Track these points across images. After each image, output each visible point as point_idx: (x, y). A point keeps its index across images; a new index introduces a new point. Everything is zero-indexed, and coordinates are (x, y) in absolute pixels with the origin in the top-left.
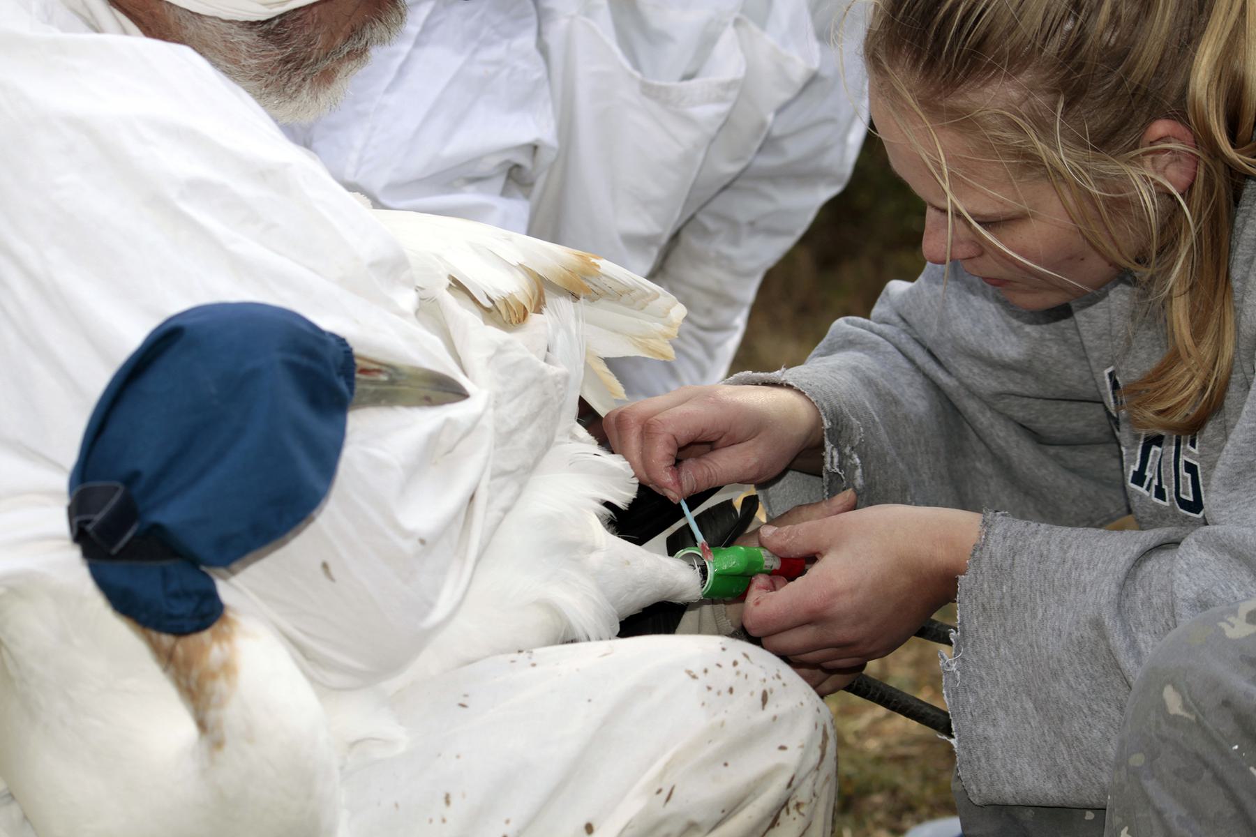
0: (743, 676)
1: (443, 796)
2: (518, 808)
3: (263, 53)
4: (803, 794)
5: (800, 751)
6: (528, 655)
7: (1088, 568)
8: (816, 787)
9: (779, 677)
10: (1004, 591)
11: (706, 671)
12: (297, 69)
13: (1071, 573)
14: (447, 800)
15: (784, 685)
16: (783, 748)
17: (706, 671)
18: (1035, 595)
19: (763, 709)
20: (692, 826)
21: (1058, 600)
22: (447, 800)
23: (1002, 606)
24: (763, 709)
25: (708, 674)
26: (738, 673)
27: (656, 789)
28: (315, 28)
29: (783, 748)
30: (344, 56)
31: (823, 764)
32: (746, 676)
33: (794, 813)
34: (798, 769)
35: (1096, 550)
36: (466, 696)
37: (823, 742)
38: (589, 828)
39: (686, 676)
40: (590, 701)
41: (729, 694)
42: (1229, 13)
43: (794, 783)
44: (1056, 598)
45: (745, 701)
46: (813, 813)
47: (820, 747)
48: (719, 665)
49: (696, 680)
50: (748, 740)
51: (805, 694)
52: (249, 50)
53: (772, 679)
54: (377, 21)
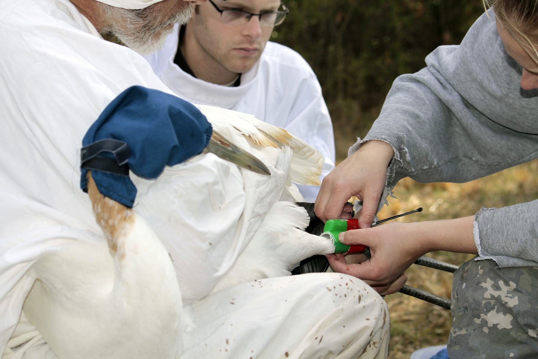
0: (350, 289)
1: (225, 340)
2: (256, 345)
3: (137, 22)
4: (376, 339)
5: (375, 320)
6: (259, 283)
7: (528, 212)
8: (382, 336)
9: (365, 290)
10: (488, 227)
11: (335, 288)
12: (148, 30)
13: (520, 215)
14: (227, 342)
15: (368, 293)
16: (368, 319)
17: (335, 288)
18: (503, 226)
19: (359, 303)
20: (331, 353)
21: (513, 226)
22: (227, 342)
23: (487, 233)
24: (359, 303)
25: (336, 289)
26: (348, 288)
27: (315, 337)
28: (158, 13)
29: (368, 319)
30: (167, 26)
31: (385, 325)
32: (352, 290)
33: (372, 346)
34: (374, 328)
35: (530, 206)
36: (233, 299)
37: (384, 317)
38: (287, 354)
39: (326, 290)
40: (286, 301)
41: (345, 297)
42: (276, 141)
43: (373, 334)
44: (512, 225)
45: (352, 299)
46: (380, 347)
47: (383, 319)
48: (340, 285)
49: (331, 292)
50: (354, 316)
51: (376, 296)
52: (131, 21)
53: (362, 291)
54: (181, 12)
